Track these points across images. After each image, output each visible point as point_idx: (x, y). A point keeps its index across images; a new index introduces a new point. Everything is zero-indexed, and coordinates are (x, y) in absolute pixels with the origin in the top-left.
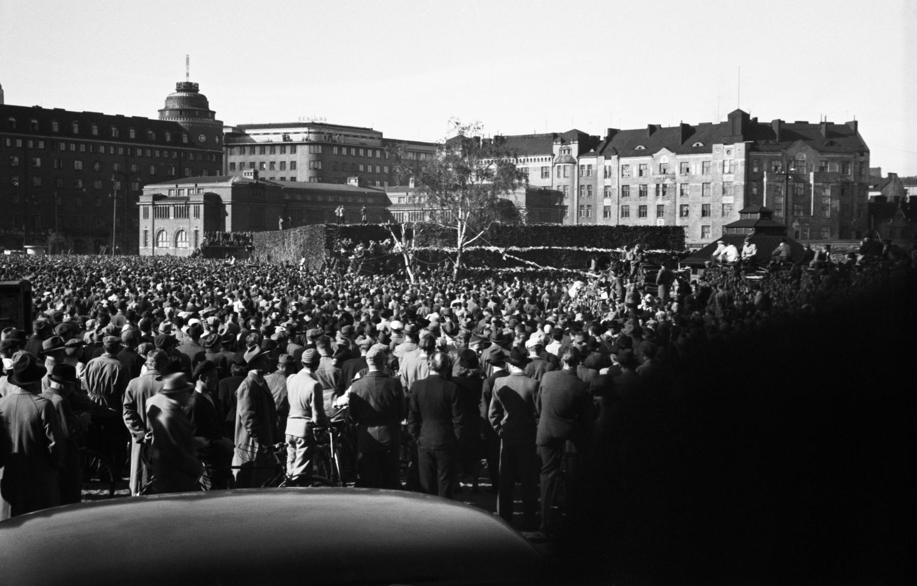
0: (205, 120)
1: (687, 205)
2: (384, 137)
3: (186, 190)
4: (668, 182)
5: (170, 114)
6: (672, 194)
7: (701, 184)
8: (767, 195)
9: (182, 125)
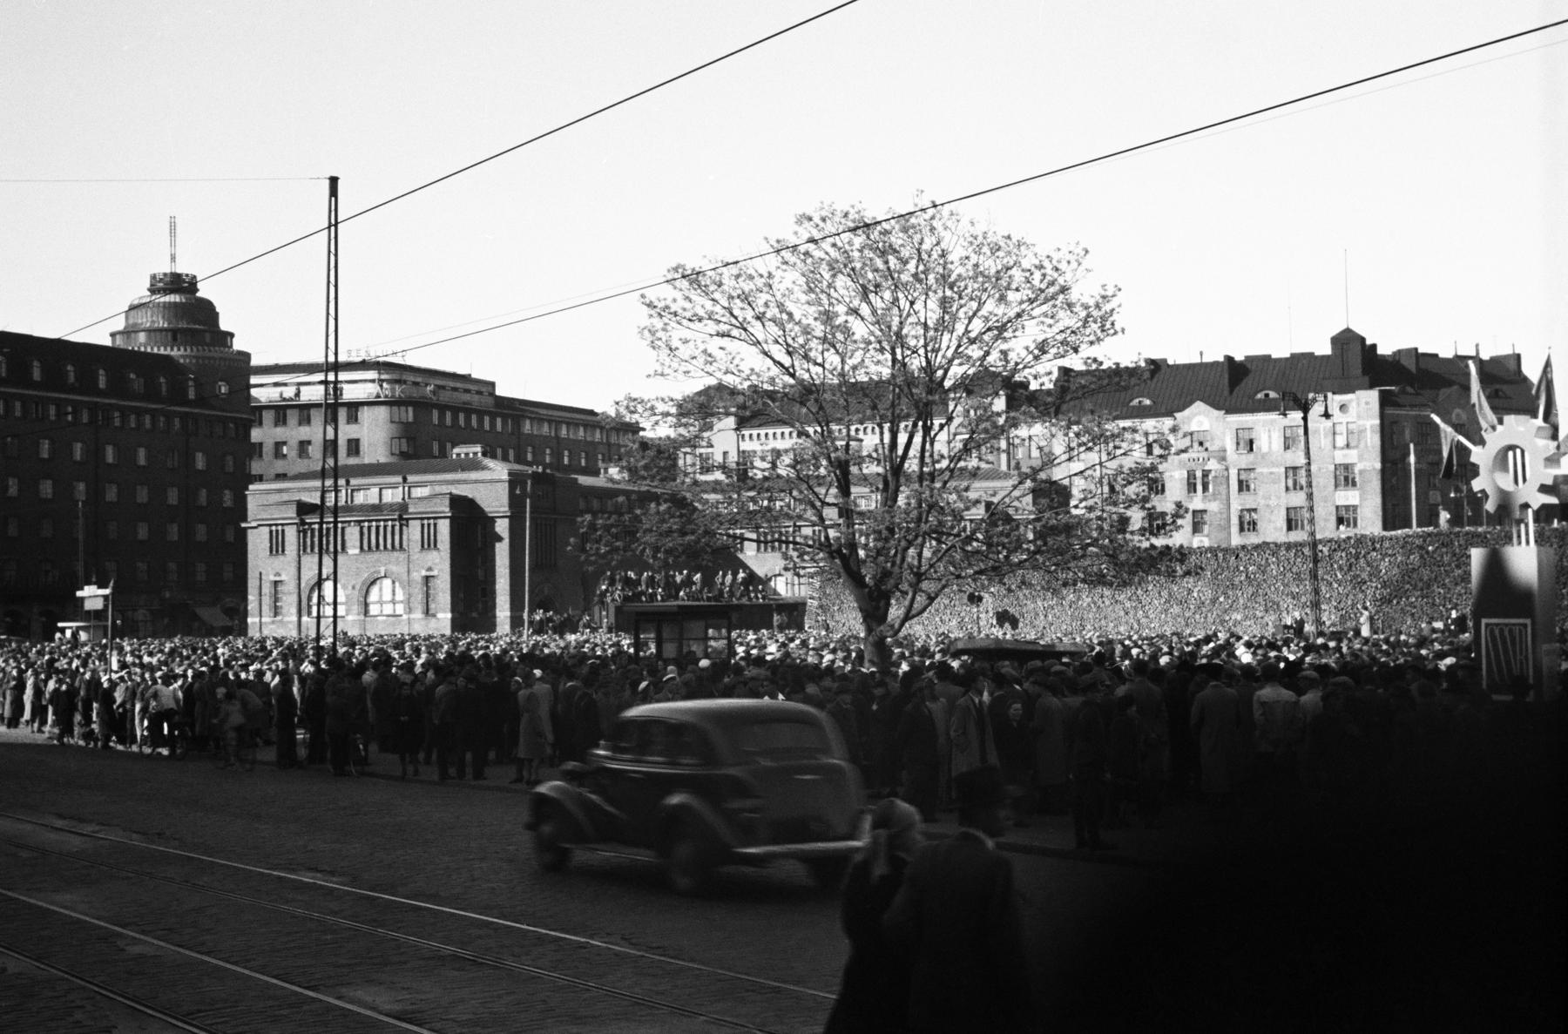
0: (216, 352)
1: (1255, 510)
2: (500, 392)
3: (375, 490)
4: (1213, 465)
5: (149, 338)
6: (1223, 489)
7: (1283, 470)
8: (1416, 487)
9: (182, 361)
